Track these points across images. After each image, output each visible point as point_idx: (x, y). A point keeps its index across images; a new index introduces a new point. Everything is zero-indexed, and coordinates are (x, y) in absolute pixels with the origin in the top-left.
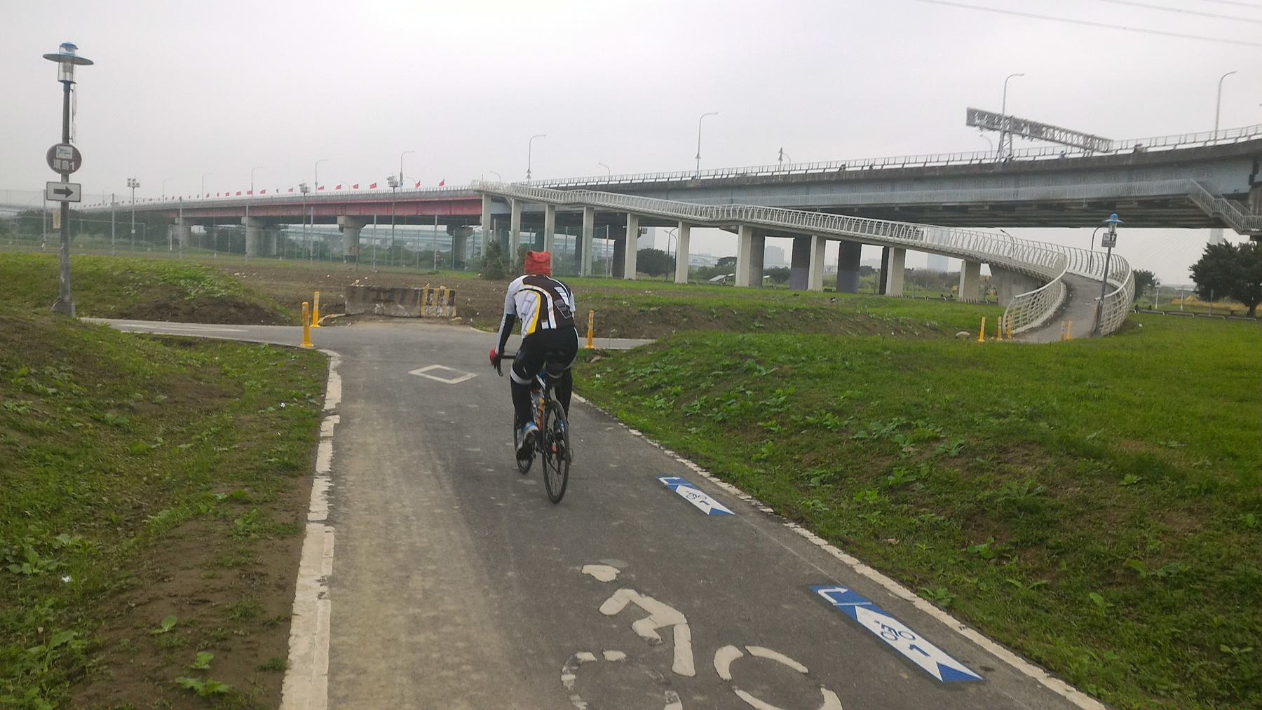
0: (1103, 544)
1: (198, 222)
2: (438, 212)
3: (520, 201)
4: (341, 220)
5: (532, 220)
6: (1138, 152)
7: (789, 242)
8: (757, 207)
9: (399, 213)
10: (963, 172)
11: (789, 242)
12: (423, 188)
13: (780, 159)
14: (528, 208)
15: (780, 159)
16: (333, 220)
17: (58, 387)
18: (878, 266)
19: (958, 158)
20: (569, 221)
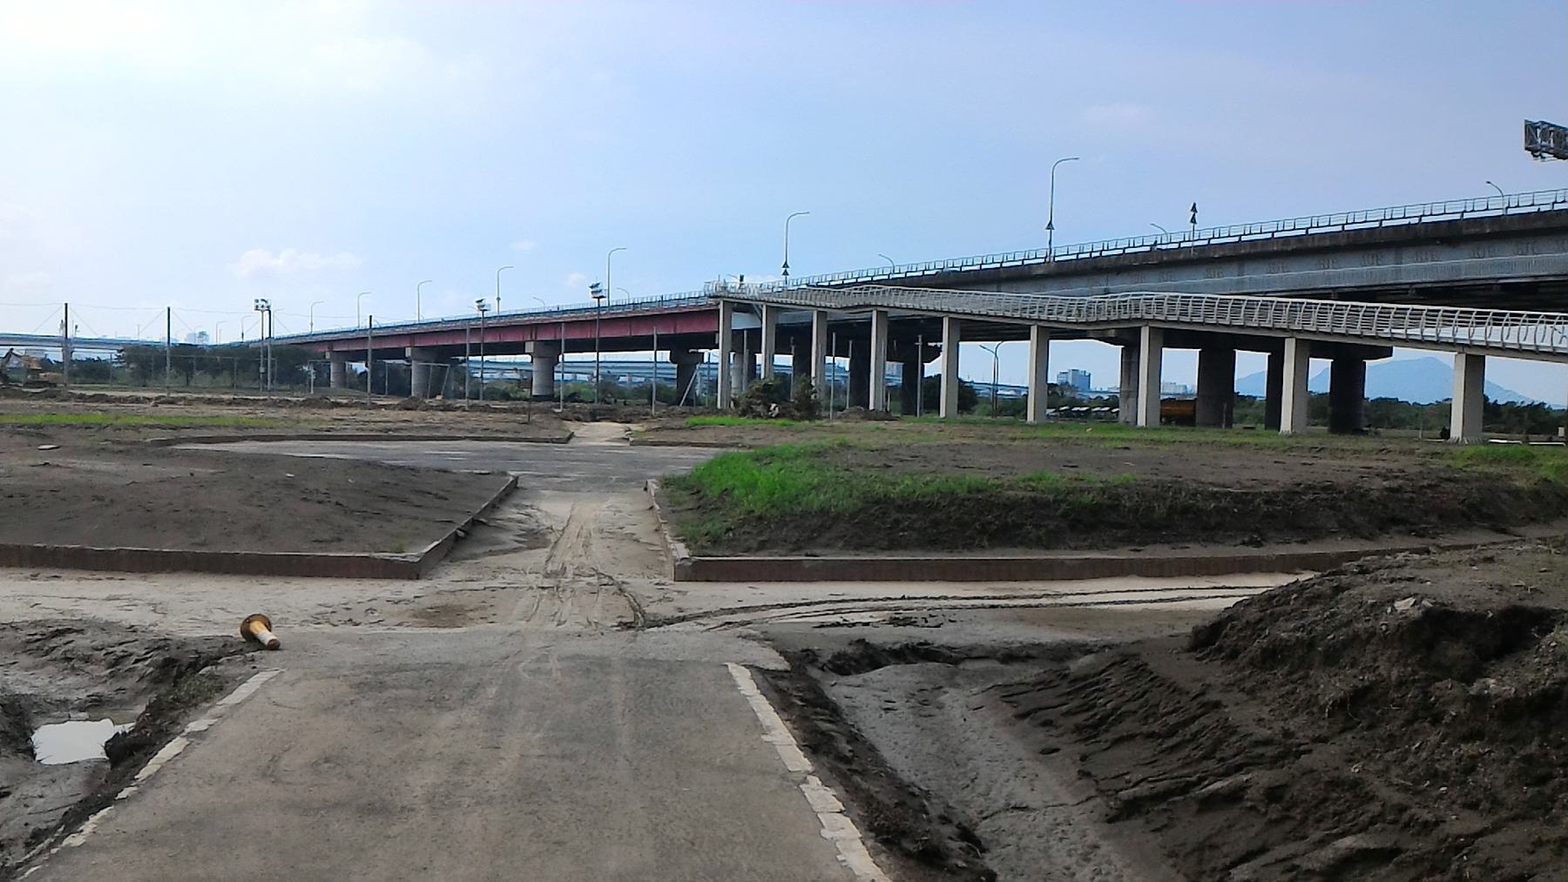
0: (1320, 727)
1: (359, 356)
2: (656, 331)
3: (775, 309)
4: (530, 347)
5: (792, 337)
6: (1154, 250)
7: (1193, 354)
8: (1205, 299)
9: (607, 333)
10: (1539, 224)
11: (1193, 354)
12: (316, 330)
13: (1193, 220)
14: (783, 319)
15: (1193, 220)
16: (518, 349)
17: (1415, 595)
18: (1260, 391)
19: (904, 270)
20: (848, 335)
